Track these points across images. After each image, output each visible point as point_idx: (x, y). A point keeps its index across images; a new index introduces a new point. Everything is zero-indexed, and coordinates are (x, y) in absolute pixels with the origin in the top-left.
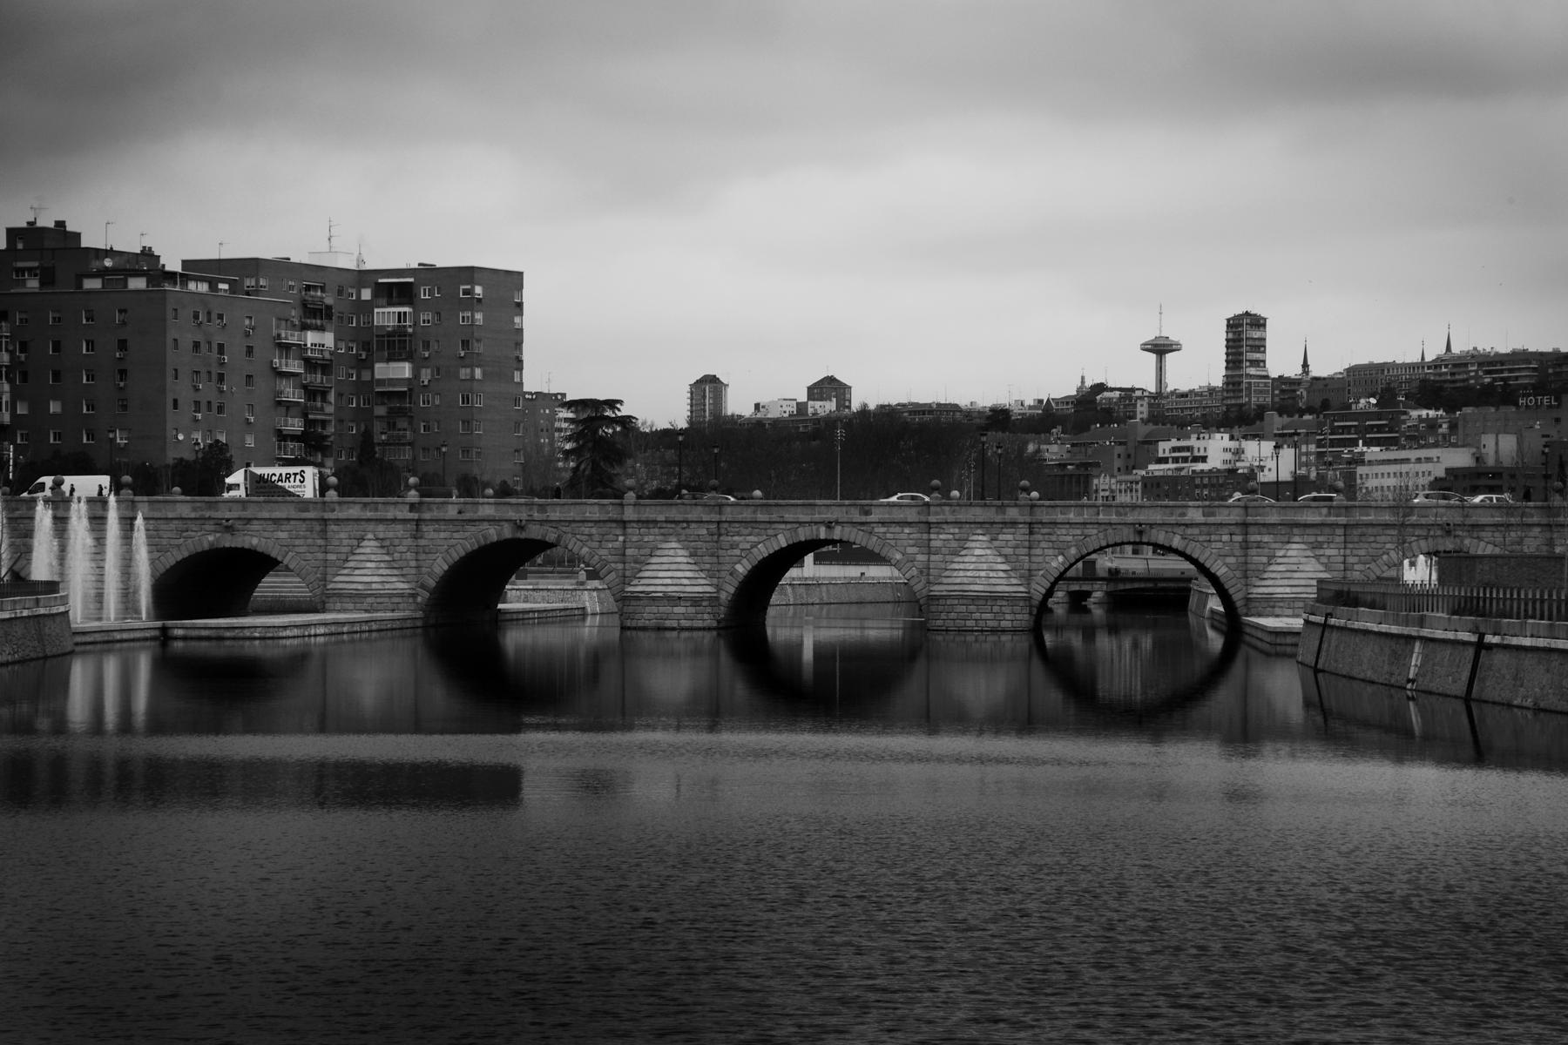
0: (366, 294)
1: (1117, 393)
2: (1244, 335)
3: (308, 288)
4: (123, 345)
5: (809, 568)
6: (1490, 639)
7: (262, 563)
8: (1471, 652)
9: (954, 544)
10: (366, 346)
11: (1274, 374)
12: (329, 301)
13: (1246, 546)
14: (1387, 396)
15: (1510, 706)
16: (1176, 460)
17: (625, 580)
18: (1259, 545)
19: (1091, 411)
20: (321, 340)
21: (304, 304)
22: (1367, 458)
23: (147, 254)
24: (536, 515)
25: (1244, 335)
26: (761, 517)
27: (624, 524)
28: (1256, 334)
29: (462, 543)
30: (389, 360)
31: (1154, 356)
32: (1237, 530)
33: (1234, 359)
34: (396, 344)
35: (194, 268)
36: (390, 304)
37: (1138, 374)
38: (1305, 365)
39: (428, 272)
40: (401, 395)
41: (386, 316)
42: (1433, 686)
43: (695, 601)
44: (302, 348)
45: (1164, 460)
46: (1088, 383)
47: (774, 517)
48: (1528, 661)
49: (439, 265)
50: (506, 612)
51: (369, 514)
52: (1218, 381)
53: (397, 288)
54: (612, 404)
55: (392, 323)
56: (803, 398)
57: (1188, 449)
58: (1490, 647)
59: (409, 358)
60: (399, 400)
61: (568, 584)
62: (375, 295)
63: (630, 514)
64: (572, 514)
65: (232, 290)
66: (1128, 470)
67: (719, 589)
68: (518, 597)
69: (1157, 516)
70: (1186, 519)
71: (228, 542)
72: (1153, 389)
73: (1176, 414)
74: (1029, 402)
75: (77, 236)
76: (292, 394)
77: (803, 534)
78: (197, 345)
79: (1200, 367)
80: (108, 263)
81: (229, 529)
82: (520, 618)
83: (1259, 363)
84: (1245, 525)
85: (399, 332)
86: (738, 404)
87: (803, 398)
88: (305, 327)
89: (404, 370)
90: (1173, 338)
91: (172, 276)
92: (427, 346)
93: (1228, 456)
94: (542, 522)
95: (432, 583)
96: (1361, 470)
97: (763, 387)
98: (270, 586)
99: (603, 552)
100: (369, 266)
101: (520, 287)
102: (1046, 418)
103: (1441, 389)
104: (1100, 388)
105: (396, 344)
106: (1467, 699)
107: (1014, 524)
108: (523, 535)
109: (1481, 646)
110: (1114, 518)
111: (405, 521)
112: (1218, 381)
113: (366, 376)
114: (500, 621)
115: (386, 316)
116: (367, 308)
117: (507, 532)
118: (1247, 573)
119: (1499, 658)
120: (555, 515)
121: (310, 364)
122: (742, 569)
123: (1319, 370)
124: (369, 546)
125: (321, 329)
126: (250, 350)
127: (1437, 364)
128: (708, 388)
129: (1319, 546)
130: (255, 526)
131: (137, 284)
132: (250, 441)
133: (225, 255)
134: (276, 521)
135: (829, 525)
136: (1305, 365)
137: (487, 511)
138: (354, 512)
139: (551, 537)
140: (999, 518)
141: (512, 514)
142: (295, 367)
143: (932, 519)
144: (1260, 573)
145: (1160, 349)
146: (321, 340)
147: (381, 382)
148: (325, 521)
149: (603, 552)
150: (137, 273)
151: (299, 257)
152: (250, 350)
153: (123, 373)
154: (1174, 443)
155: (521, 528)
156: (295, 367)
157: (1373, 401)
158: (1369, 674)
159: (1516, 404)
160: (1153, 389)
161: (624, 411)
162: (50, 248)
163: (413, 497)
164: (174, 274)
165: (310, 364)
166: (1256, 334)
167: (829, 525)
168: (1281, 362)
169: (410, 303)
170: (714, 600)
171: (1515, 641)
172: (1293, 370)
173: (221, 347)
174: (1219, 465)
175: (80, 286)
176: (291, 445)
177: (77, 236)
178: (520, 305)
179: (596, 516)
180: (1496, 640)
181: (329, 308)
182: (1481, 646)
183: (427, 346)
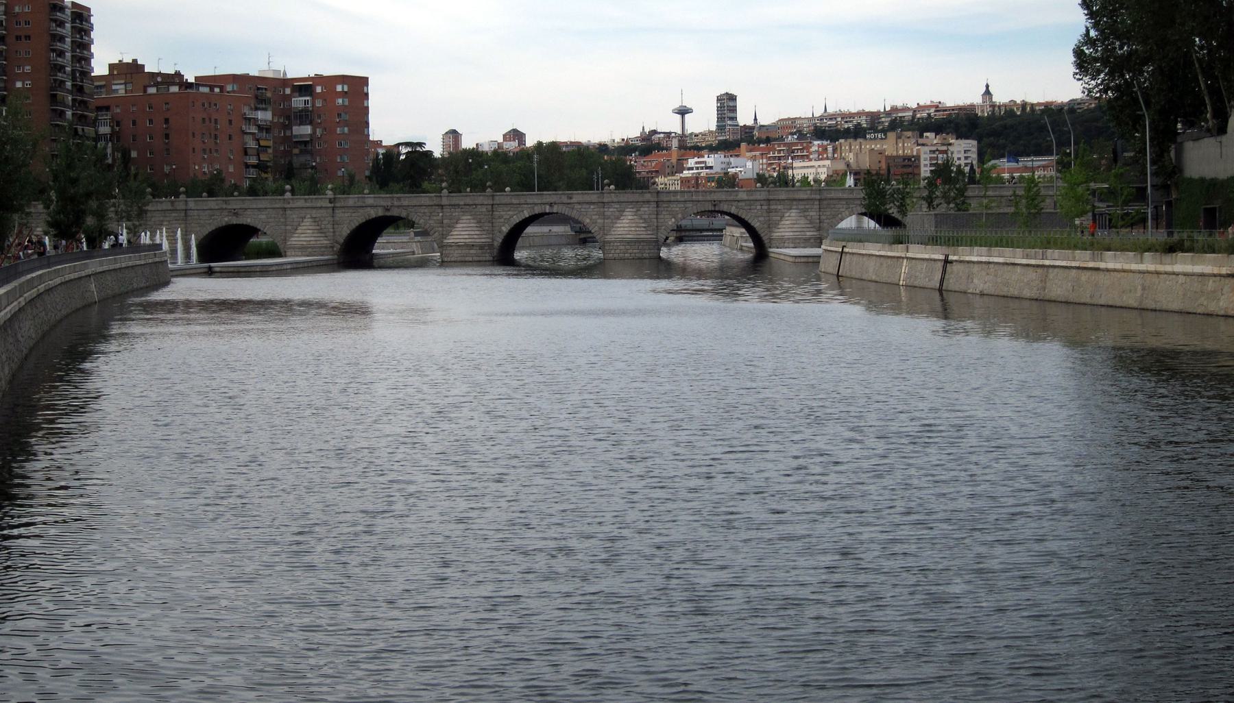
0: (288, 91)
2: (727, 104)
4: (167, 121)
5: (530, 230)
6: (951, 258)
7: (253, 231)
8: (940, 265)
10: (288, 118)
13: (769, 211)
14: (801, 135)
15: (965, 293)
17: (444, 236)
18: (776, 211)
19: (649, 144)
20: (265, 116)
21: (256, 97)
23: (178, 75)
24: (396, 203)
25: (727, 104)
26: (515, 201)
27: (442, 206)
28: (731, 104)
29: (358, 219)
30: (301, 124)
31: (679, 116)
33: (721, 118)
34: (304, 117)
35: (201, 81)
36: (300, 96)
37: (671, 124)
38: (755, 119)
39: (319, 79)
40: (306, 143)
41: (299, 102)
42: (916, 283)
43: (481, 247)
44: (256, 120)
45: (690, 169)
46: (647, 130)
47: (522, 201)
48: (976, 268)
49: (325, 74)
50: (377, 254)
51: (308, 205)
53: (304, 87)
54: (421, 144)
55: (302, 106)
56: (501, 140)
58: (951, 262)
59: (311, 123)
60: (305, 145)
61: (405, 239)
62: (293, 91)
63: (445, 201)
64: (415, 202)
66: (673, 174)
67: (493, 240)
69: (723, 197)
71: (235, 221)
72: (680, 132)
73: (690, 146)
74: (618, 140)
75: (143, 66)
76: (252, 144)
77: (537, 210)
79: (703, 121)
80: (159, 79)
81: (236, 214)
83: (734, 119)
84: (769, 200)
85: (305, 110)
86: (467, 143)
87: (501, 140)
88: (257, 109)
89: (307, 130)
90: (689, 106)
91: (190, 85)
92: (319, 117)
94: (398, 207)
95: (342, 241)
97: (481, 135)
100: (289, 76)
101: (367, 85)
102: (627, 148)
104: (654, 132)
105: (304, 117)
106: (940, 290)
107: (648, 202)
108: (388, 214)
109: (947, 261)
110: (700, 198)
111: (327, 208)
112: (713, 128)
113: (288, 133)
115: (299, 102)
116: (289, 98)
117: (381, 213)
118: (771, 226)
119: (956, 267)
120: (406, 203)
121: (260, 128)
123: (764, 120)
124: (307, 222)
125: (265, 109)
126: (230, 122)
127: (821, 118)
128: (454, 135)
129: (806, 210)
130: (249, 212)
131: (174, 89)
132: (231, 169)
133: (218, 73)
134: (259, 209)
135: (551, 205)
136: (755, 119)
137: (370, 201)
138: (301, 203)
139: (404, 214)
140: (641, 199)
141: (383, 203)
142: (254, 130)
144: (777, 224)
145: (683, 112)
146: (265, 116)
147: (296, 136)
148: (285, 209)
150: (174, 84)
152: (230, 122)
153: (167, 136)
154: (696, 159)
155: (388, 210)
156: (254, 130)
157: (346, 129)
158: (874, 278)
159: (865, 137)
160: (680, 132)
161: (427, 148)
163: (330, 194)
164: (192, 84)
165: (260, 128)
166: (731, 104)
167: (551, 205)
168: (744, 118)
169: (311, 95)
170: (491, 246)
171: (967, 258)
172: (750, 122)
174: (719, 170)
175: (145, 91)
176: (252, 170)
177: (143, 66)
178: (367, 94)
179: (428, 203)
180: (955, 258)
182: (947, 261)
183: (319, 117)
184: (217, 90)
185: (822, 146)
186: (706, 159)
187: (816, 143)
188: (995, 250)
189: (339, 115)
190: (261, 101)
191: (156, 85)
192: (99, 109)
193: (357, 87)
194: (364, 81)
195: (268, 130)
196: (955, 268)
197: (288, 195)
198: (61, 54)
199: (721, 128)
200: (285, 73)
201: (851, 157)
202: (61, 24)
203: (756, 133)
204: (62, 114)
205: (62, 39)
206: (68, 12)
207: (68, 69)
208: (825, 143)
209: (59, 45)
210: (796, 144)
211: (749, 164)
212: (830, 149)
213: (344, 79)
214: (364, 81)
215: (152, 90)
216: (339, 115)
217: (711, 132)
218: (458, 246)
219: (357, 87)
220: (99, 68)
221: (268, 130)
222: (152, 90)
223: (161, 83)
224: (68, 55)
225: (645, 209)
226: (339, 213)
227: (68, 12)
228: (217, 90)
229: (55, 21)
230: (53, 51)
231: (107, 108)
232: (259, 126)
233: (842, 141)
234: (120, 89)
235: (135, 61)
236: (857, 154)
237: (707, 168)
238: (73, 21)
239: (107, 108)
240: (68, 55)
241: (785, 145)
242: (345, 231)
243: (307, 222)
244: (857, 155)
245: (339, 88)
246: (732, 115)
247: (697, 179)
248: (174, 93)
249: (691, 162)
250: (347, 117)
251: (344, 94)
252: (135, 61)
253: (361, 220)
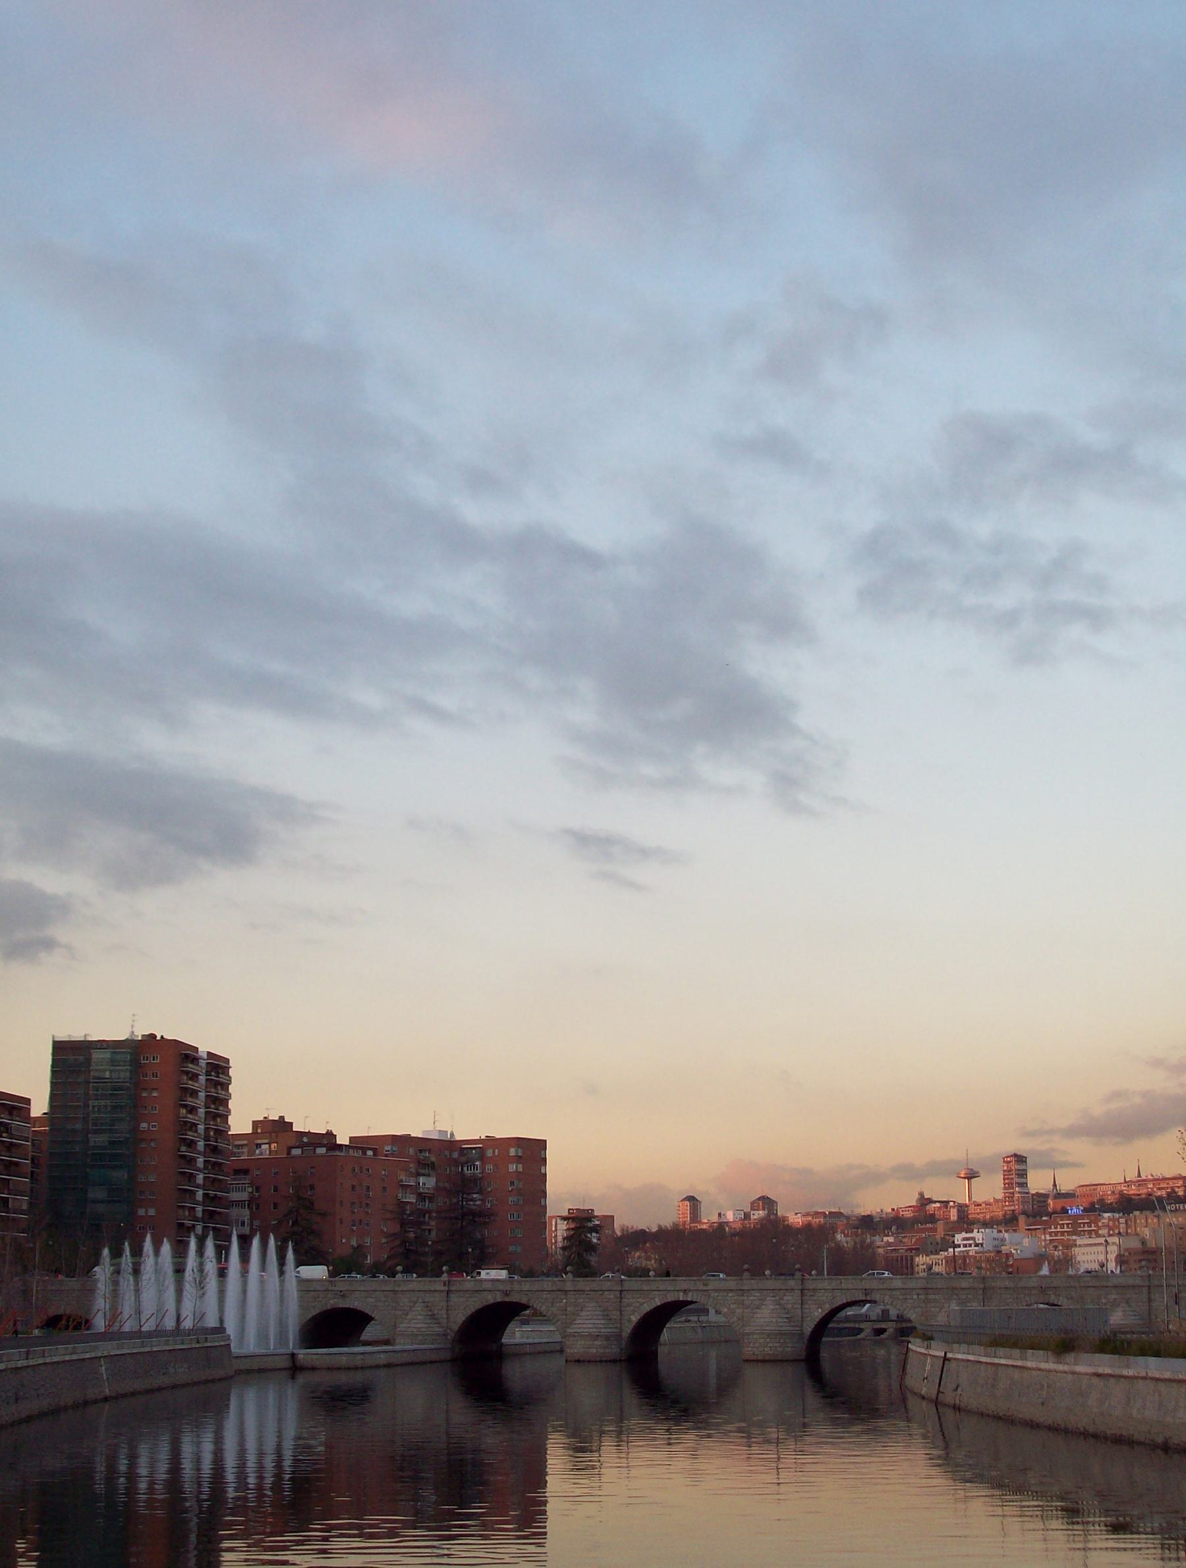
1: (938, 1205)
3: (421, 1151)
9: (757, 1303)
11: (1033, 1192)
12: (433, 1159)
16: (965, 1246)
20: (428, 1183)
22: (1078, 1243)
23: (330, 1135)
26: (645, 1288)
32: (921, 1292)
33: (1008, 1185)
38: (1055, 1185)
43: (607, 1338)
52: (1000, 1196)
57: (973, 1238)
58: (949, 1360)
63: (569, 1286)
64: (537, 1287)
65: (375, 1154)
66: (937, 1253)
68: (516, 1334)
70: (892, 1286)
71: (342, 1304)
78: (353, 1187)
79: (989, 1189)
80: (305, 1139)
82: (520, 1353)
83: (1023, 1185)
88: (418, 1174)
91: (340, 1147)
93: (996, 1243)
95: (456, 1328)
96: (1076, 1250)
98: (369, 1333)
99: (554, 1309)
100: (458, 1138)
103: (1131, 1199)
108: (507, 1299)
109: (945, 1359)
112: (1000, 1196)
114: (500, 1355)
122: (635, 1319)
125: (429, 1175)
131: (321, 1151)
136: (1055, 1185)
139: (524, 1301)
143: (745, 1288)
146: (428, 1183)
149: (554, 1309)
150: (321, 1145)
151: (416, 1133)
152: (384, 1188)
154: (964, 1235)
162: (137, 1131)
168: (1038, 1182)
170: (619, 1337)
173: (368, 1188)
175: (289, 1153)
181: (433, 1163)
182: (945, 1359)
184: (370, 1153)
185: (1113, 1220)
186: (975, 1234)
187: (1106, 1215)
188: (1001, 1351)
189: (512, 1183)
190: (425, 1166)
191: (301, 1146)
192: (238, 1172)
193: (532, 1152)
194: (542, 1144)
195: (431, 1199)
196: (953, 1365)
197: (399, 1276)
198: (192, 1110)
199: (1010, 1197)
200: (452, 1135)
201: (1146, 1233)
202: (194, 1077)
203: (972, 1209)
204: (192, 1177)
205: (194, 1093)
206: (203, 1063)
207: (201, 1127)
208: (1117, 1215)
209: (190, 1101)
210: (1082, 1217)
211: (1026, 1242)
212: (1122, 1221)
213: (519, 1142)
214: (542, 1144)
215: (296, 1152)
216: (512, 1183)
217: (996, 1201)
218: (581, 1336)
219: (532, 1152)
220: (240, 1123)
221: (431, 1199)
222: (296, 1152)
223: (307, 1144)
224: (202, 1111)
225: (788, 1298)
226: (454, 1298)
227: (203, 1063)
228: (370, 1153)
229: (187, 1073)
230: (185, 1106)
231: (246, 1172)
232: (420, 1194)
233: (1137, 1213)
234: (265, 1150)
235: (282, 1118)
236: (1148, 1229)
237: (977, 1245)
238: (208, 1073)
239: (246, 1172)
240: (202, 1111)
241: (1069, 1217)
242: (459, 1317)
243: (419, 1307)
244: (1154, 1231)
245: (512, 1152)
246: (1022, 1180)
247: (964, 1258)
248: (322, 1156)
249: (958, 1238)
250: (521, 1186)
251: (518, 1159)
252: (282, 1118)
253: (478, 1306)
